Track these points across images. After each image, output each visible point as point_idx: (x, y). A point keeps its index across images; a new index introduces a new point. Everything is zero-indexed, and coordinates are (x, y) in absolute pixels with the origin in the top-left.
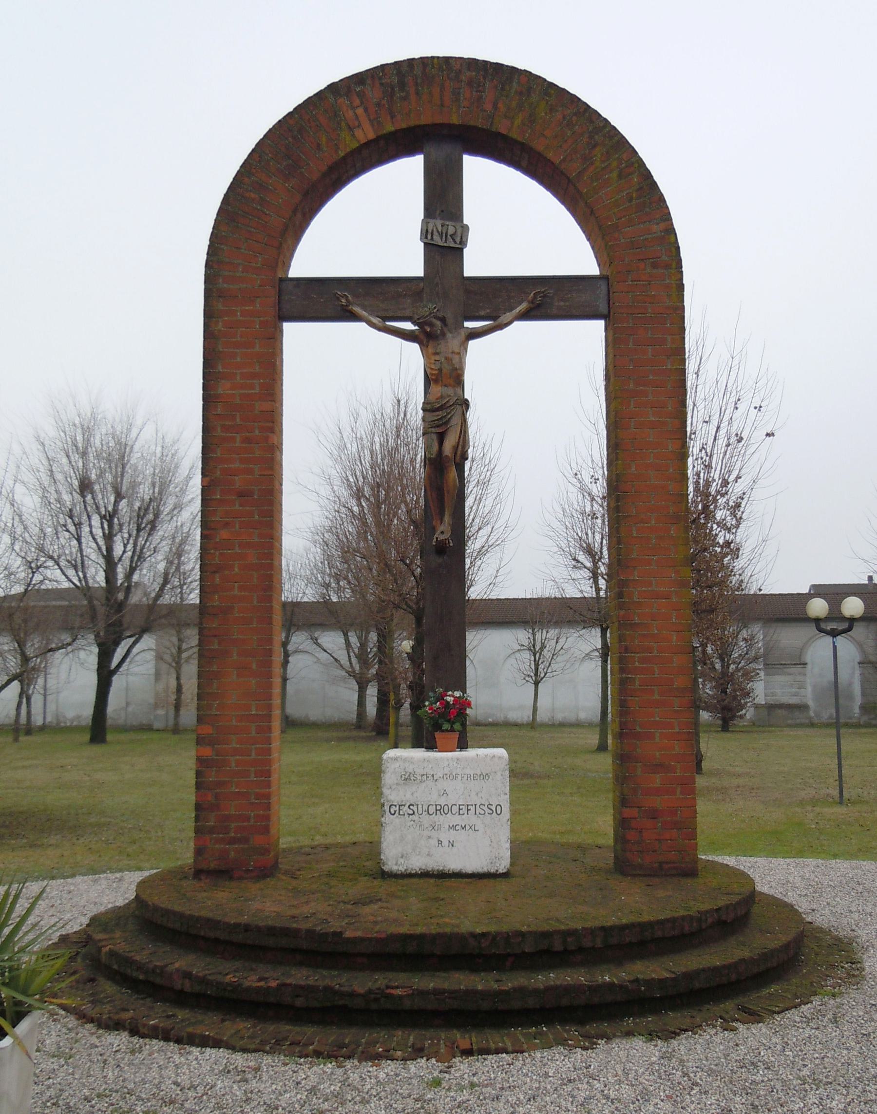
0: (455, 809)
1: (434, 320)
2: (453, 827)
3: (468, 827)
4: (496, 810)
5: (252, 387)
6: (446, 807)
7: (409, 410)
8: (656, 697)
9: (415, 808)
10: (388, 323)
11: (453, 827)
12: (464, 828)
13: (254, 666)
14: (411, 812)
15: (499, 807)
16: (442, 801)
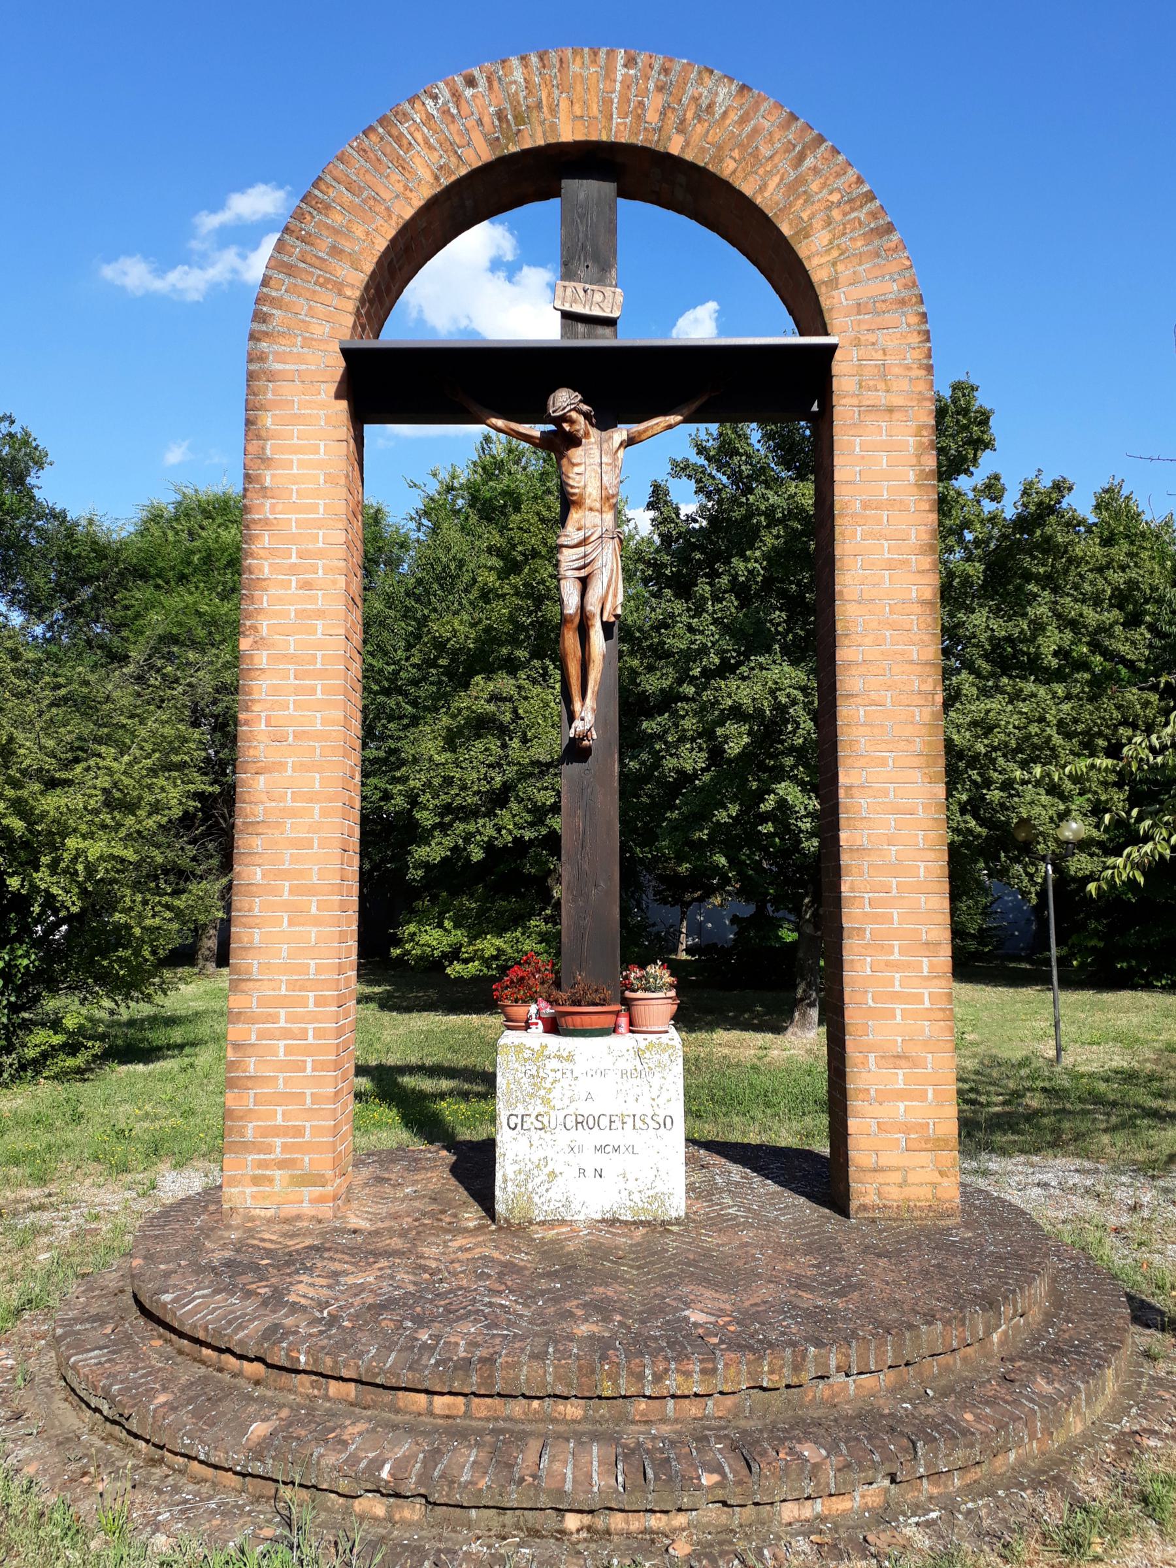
0: (604, 1122)
1: (574, 415)
2: (600, 1149)
3: (623, 1149)
4: (666, 1123)
5: (314, 508)
6: (591, 1124)
7: (577, 1019)
8: (896, 956)
9: (545, 1120)
10: (704, 399)
11: (600, 1149)
12: (617, 1150)
13: (314, 910)
14: (539, 1125)
15: (668, 1120)
16: (586, 1109)
